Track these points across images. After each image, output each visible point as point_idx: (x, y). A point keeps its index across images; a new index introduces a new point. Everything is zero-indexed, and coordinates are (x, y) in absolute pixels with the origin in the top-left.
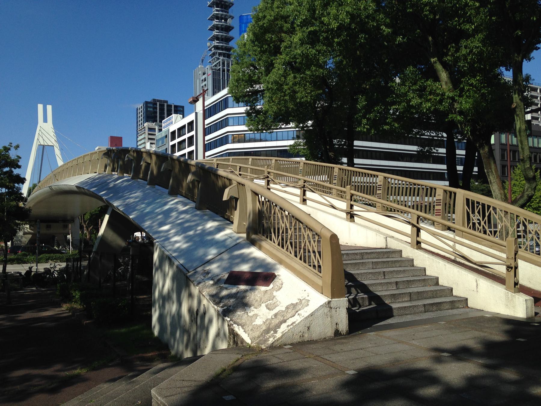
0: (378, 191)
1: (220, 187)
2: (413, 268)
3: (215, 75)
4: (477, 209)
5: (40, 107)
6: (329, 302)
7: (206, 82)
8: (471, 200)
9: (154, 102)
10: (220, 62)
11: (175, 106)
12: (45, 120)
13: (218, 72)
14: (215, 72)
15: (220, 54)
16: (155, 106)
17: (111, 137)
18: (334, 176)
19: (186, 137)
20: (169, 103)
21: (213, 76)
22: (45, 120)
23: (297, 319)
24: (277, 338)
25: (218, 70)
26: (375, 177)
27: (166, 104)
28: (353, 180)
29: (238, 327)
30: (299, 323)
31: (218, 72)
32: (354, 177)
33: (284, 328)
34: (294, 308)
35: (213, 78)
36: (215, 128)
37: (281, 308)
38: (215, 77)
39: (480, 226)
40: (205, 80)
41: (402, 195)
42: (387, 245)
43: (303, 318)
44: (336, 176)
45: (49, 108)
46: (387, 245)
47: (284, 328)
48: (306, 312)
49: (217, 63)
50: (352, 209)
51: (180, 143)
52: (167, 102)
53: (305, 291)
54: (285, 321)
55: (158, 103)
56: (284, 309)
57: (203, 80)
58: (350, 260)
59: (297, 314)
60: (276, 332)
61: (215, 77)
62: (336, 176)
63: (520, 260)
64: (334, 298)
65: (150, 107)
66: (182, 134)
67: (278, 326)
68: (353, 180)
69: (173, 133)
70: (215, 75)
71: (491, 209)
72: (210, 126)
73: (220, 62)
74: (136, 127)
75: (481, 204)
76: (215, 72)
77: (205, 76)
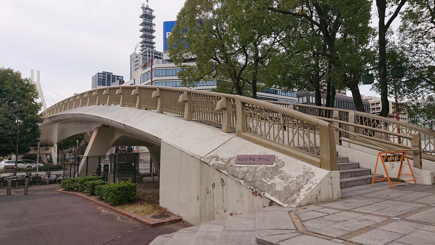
0: (337, 117)
1: (37, 107)
2: (358, 170)
4: (364, 122)
6: (112, 74)
7: (136, 68)
8: (364, 117)
9: (104, 73)
10: (147, 51)
11: (118, 76)
15: (147, 46)
16: (105, 81)
17: (31, 70)
20: (113, 74)
27: (111, 75)
39: (367, 133)
40: (137, 61)
49: (145, 52)
52: (112, 73)
55: (106, 74)
57: (136, 61)
65: (101, 81)
71: (375, 121)
73: (147, 51)
75: (367, 118)
77: (138, 58)
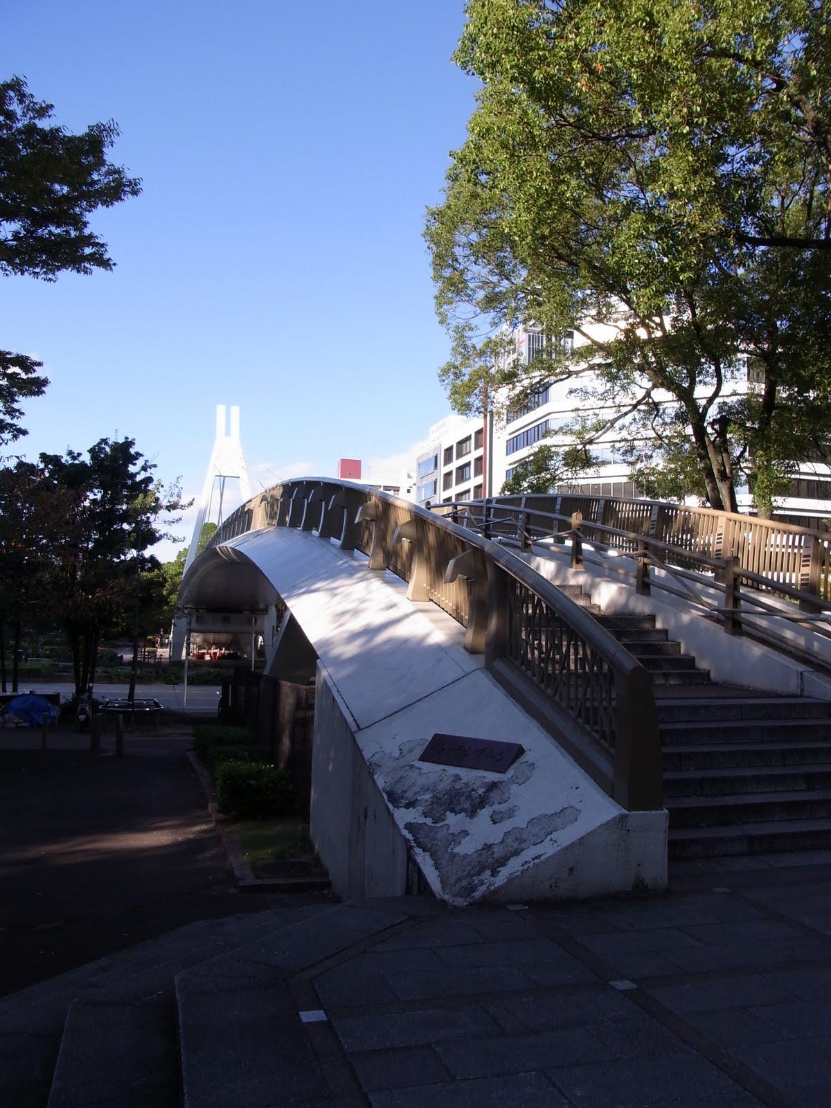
3: (533, 342)
5: (221, 409)
6: (622, 819)
12: (228, 433)
13: (539, 337)
14: (533, 336)
18: (718, 535)
19: (471, 457)
21: (529, 345)
22: (228, 433)
23: (547, 849)
24: (496, 886)
25: (538, 333)
26: (779, 533)
28: (772, 542)
29: (423, 854)
30: (547, 860)
31: (539, 337)
32: (773, 535)
33: (514, 866)
34: (547, 824)
35: (529, 348)
36: (515, 443)
37: (520, 820)
38: (533, 345)
41: (782, 570)
42: (802, 690)
43: (559, 848)
44: (722, 534)
45: (235, 410)
46: (802, 690)
47: (514, 866)
48: (566, 836)
50: (736, 607)
51: (461, 469)
53: (577, 788)
54: (517, 853)
56: (524, 825)
58: (716, 721)
59: (549, 837)
60: (494, 873)
61: (533, 345)
62: (722, 534)
63: (379, 786)
64: (656, 810)
66: (464, 452)
67: (503, 862)
68: (772, 542)
69: (449, 451)
70: (533, 342)
72: (517, 437)
74: (516, 460)
76: (533, 336)
